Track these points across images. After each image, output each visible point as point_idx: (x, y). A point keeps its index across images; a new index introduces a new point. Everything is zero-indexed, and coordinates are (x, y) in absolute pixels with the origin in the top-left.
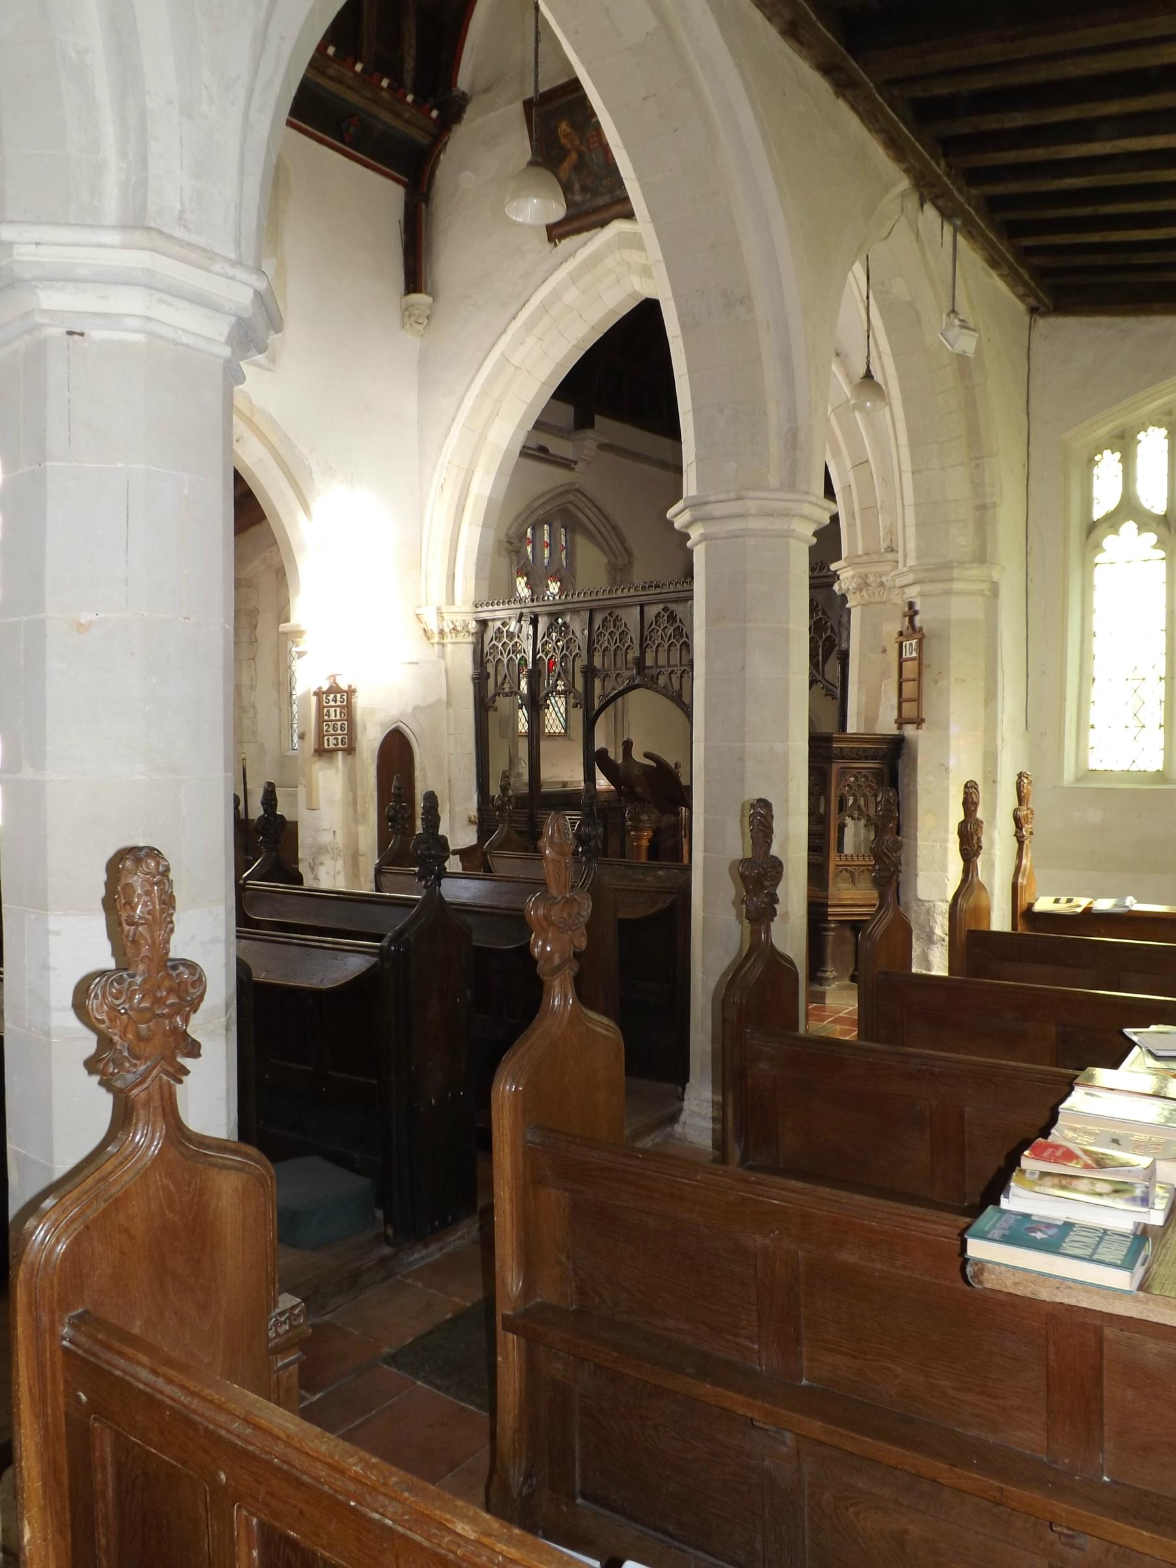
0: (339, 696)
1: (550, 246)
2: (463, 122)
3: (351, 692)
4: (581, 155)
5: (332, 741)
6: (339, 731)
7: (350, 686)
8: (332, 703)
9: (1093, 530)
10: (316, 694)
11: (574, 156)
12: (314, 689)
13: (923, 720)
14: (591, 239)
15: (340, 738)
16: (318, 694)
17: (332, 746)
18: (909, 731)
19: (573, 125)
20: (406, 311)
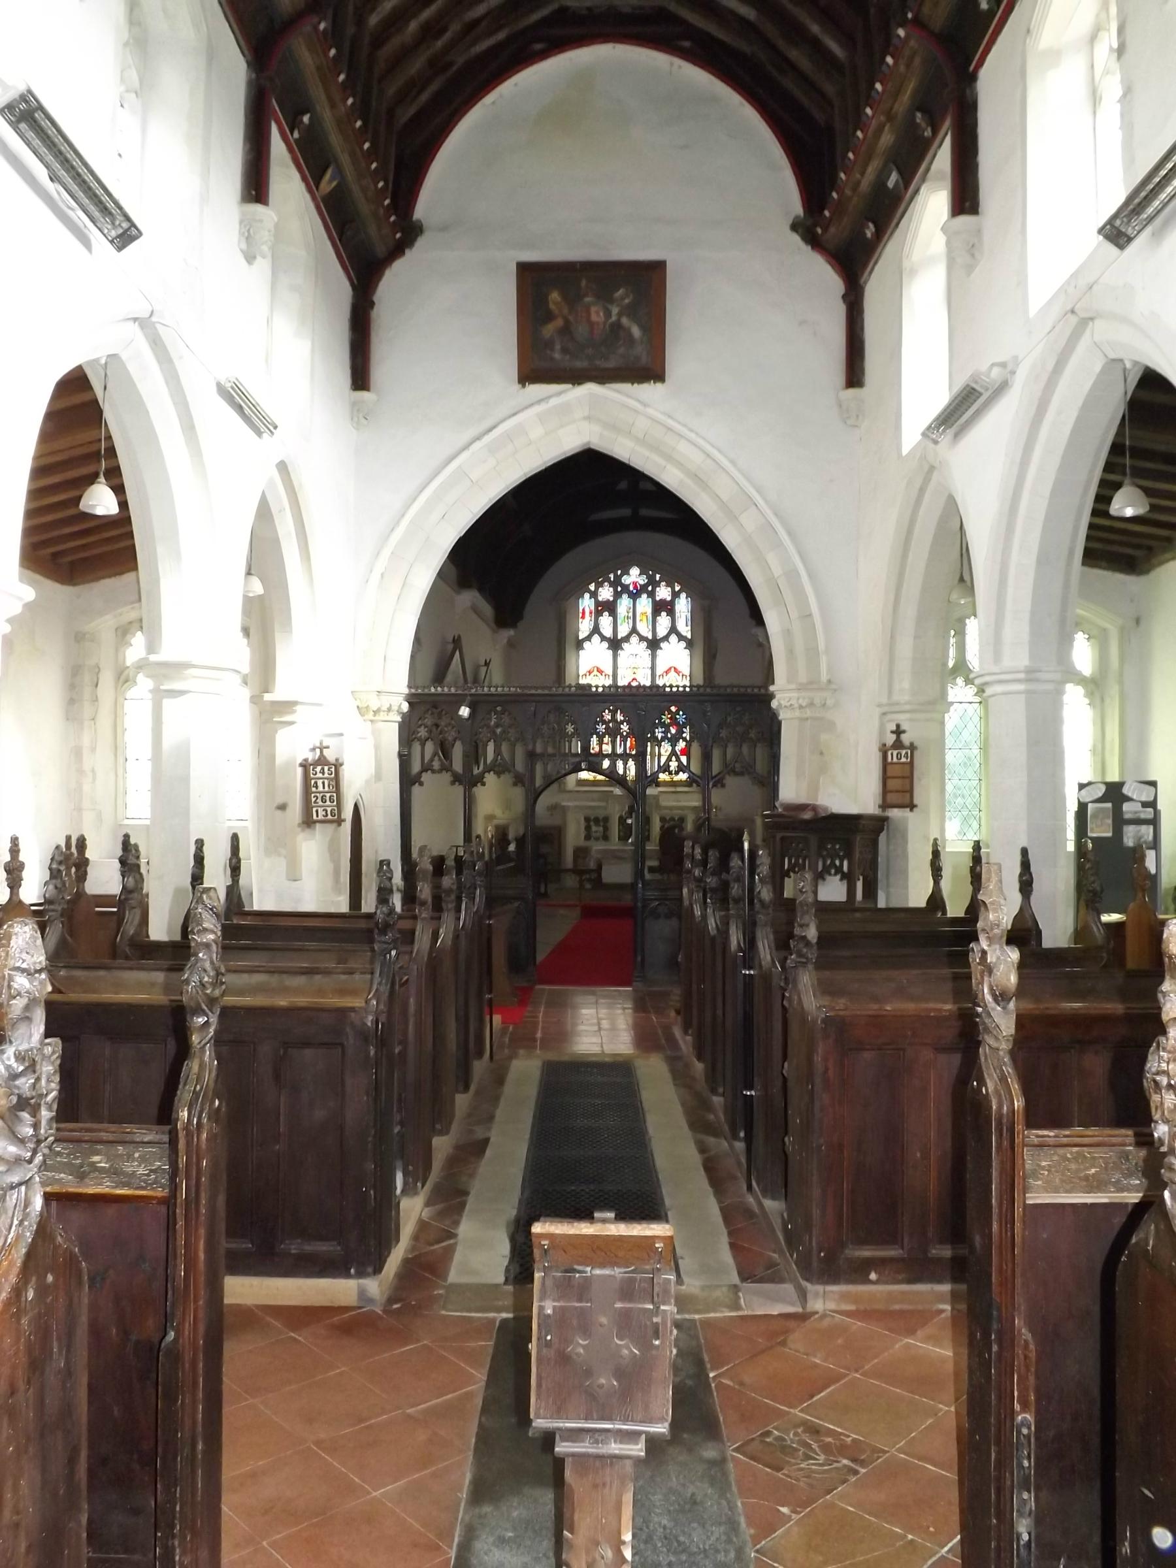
0: (326, 768)
1: (517, 386)
2: (414, 249)
3: (338, 765)
4: (567, 321)
5: (321, 813)
6: (328, 803)
7: (337, 760)
8: (320, 775)
9: (579, 645)
10: (301, 765)
11: (559, 322)
12: (299, 761)
13: (916, 806)
14: (559, 394)
15: (329, 809)
16: (305, 765)
17: (320, 817)
18: (894, 813)
19: (565, 297)
20: (355, 406)
